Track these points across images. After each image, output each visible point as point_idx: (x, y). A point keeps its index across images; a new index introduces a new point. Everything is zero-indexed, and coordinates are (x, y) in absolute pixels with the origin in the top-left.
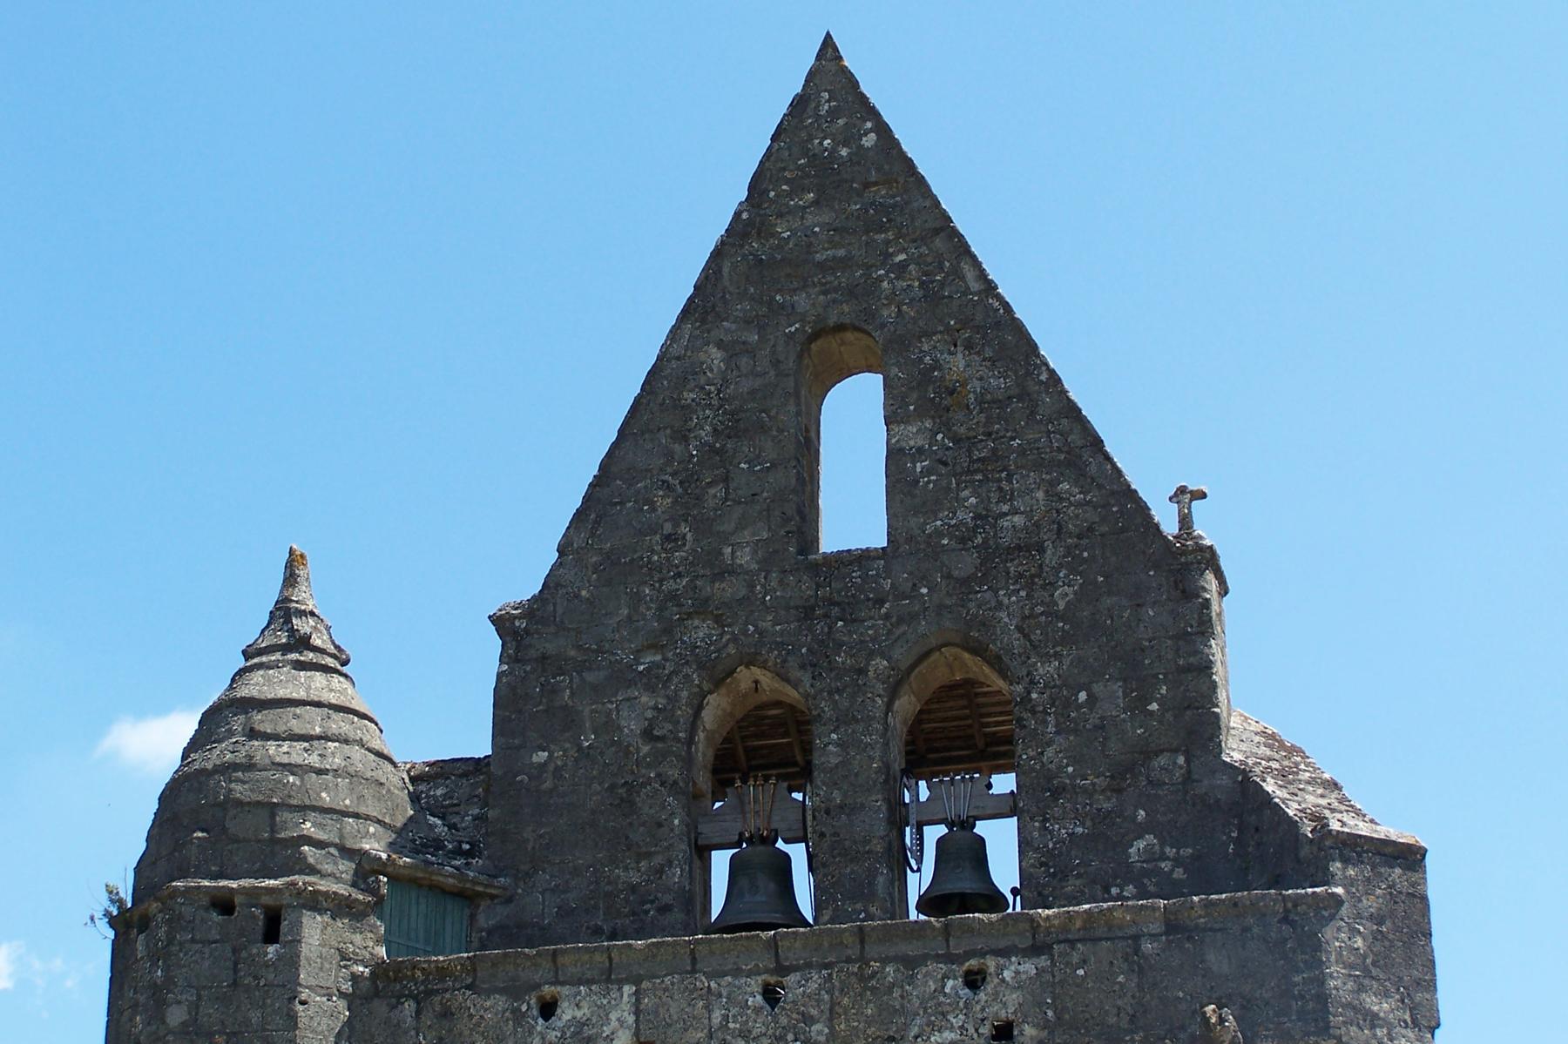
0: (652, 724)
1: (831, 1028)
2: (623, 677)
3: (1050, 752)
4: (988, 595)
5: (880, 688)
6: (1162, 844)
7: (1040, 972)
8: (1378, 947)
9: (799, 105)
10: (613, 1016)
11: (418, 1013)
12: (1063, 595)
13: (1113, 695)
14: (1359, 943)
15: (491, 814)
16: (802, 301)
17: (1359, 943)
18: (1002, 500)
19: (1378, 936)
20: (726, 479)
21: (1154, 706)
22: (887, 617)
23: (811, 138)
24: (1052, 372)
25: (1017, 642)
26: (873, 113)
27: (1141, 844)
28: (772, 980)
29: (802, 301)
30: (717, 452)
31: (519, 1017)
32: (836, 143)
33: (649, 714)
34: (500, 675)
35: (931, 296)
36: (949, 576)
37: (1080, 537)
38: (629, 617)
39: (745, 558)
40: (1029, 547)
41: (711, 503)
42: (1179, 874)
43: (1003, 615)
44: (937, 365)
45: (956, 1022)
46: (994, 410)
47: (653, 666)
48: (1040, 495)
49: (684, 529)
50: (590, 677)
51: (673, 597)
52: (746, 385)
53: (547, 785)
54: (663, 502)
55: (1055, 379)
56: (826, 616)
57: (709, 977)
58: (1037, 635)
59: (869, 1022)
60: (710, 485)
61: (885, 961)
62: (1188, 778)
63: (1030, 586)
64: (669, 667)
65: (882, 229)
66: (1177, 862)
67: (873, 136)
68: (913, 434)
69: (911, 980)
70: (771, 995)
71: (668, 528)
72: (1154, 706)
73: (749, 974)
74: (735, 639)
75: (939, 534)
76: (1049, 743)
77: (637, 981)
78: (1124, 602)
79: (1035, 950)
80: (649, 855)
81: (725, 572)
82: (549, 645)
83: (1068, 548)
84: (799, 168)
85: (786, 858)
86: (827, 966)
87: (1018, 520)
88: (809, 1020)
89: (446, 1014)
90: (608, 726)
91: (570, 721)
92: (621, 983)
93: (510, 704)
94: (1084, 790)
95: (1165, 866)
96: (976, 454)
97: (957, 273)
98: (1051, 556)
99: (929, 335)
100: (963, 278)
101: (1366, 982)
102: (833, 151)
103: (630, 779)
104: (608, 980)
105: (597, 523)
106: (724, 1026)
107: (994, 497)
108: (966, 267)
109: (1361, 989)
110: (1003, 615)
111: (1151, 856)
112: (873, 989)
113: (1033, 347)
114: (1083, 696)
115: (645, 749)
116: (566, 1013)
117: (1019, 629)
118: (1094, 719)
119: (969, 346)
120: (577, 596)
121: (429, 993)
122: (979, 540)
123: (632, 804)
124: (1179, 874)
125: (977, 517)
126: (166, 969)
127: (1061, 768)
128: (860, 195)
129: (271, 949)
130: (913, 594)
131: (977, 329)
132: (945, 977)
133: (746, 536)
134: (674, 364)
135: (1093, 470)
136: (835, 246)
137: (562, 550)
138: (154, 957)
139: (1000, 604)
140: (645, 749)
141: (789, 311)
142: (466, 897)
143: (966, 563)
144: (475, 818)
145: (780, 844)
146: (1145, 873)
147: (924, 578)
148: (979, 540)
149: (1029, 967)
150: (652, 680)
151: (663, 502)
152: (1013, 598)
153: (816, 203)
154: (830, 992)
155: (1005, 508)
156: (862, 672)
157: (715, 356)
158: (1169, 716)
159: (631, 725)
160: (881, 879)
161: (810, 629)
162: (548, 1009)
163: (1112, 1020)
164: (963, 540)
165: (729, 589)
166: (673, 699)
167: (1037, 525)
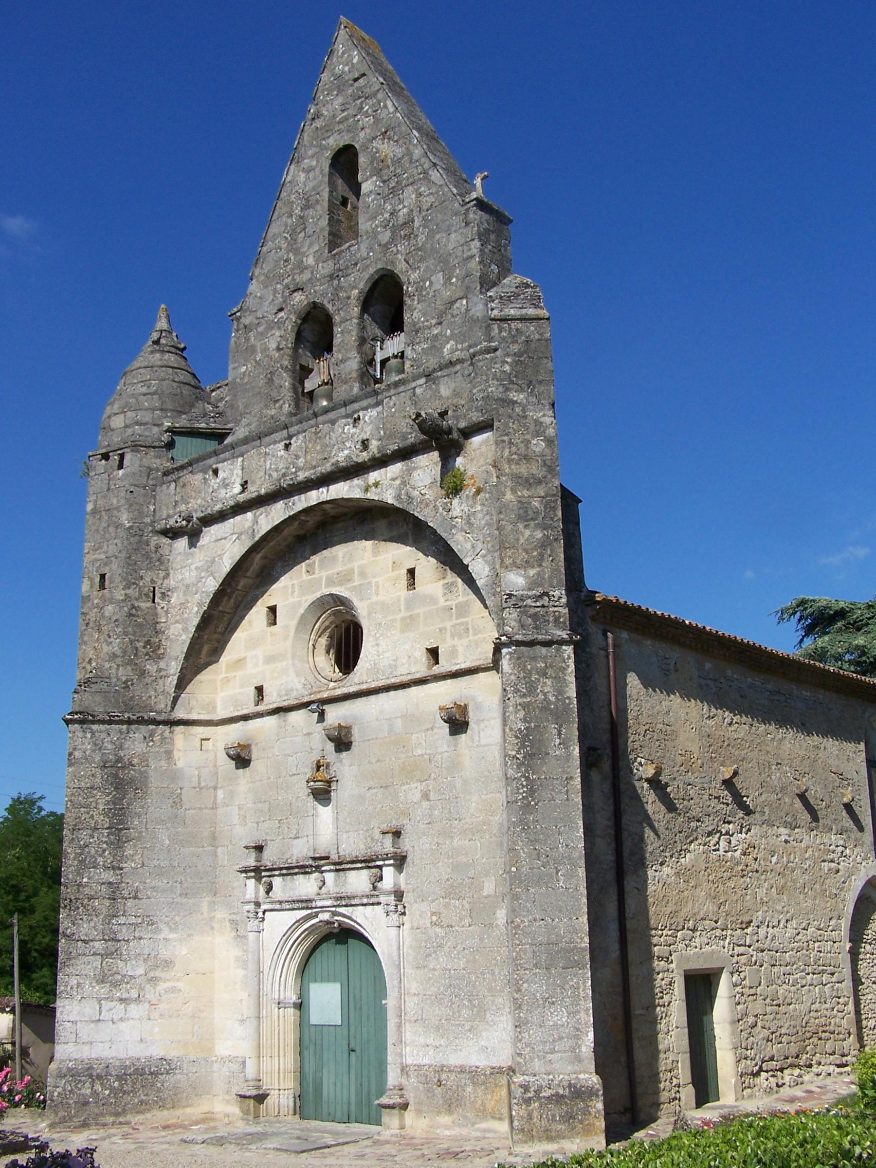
8: (519, 368)
10: (235, 472)
12: (422, 238)
14: (507, 368)
17: (507, 368)
21: (454, 280)
27: (448, 346)
28: (287, 442)
32: (344, 66)
33: (279, 339)
36: (380, 245)
38: (273, 300)
45: (348, 445)
50: (260, 329)
52: (311, 184)
53: (246, 381)
62: (467, 310)
69: (333, 430)
70: (287, 447)
73: (279, 442)
75: (377, 226)
87: (405, 210)
90: (266, 349)
92: (238, 457)
96: (391, 186)
101: (511, 386)
103: (271, 369)
104: (234, 457)
109: (507, 389)
114: (428, 283)
115: (277, 355)
116: (221, 474)
117: (405, 260)
122: (391, 225)
127: (419, 319)
128: (352, 85)
129: (121, 472)
148: (391, 225)
154: (305, 443)
155: (401, 207)
158: (460, 283)
162: (216, 472)
164: (385, 227)
165: (306, 276)
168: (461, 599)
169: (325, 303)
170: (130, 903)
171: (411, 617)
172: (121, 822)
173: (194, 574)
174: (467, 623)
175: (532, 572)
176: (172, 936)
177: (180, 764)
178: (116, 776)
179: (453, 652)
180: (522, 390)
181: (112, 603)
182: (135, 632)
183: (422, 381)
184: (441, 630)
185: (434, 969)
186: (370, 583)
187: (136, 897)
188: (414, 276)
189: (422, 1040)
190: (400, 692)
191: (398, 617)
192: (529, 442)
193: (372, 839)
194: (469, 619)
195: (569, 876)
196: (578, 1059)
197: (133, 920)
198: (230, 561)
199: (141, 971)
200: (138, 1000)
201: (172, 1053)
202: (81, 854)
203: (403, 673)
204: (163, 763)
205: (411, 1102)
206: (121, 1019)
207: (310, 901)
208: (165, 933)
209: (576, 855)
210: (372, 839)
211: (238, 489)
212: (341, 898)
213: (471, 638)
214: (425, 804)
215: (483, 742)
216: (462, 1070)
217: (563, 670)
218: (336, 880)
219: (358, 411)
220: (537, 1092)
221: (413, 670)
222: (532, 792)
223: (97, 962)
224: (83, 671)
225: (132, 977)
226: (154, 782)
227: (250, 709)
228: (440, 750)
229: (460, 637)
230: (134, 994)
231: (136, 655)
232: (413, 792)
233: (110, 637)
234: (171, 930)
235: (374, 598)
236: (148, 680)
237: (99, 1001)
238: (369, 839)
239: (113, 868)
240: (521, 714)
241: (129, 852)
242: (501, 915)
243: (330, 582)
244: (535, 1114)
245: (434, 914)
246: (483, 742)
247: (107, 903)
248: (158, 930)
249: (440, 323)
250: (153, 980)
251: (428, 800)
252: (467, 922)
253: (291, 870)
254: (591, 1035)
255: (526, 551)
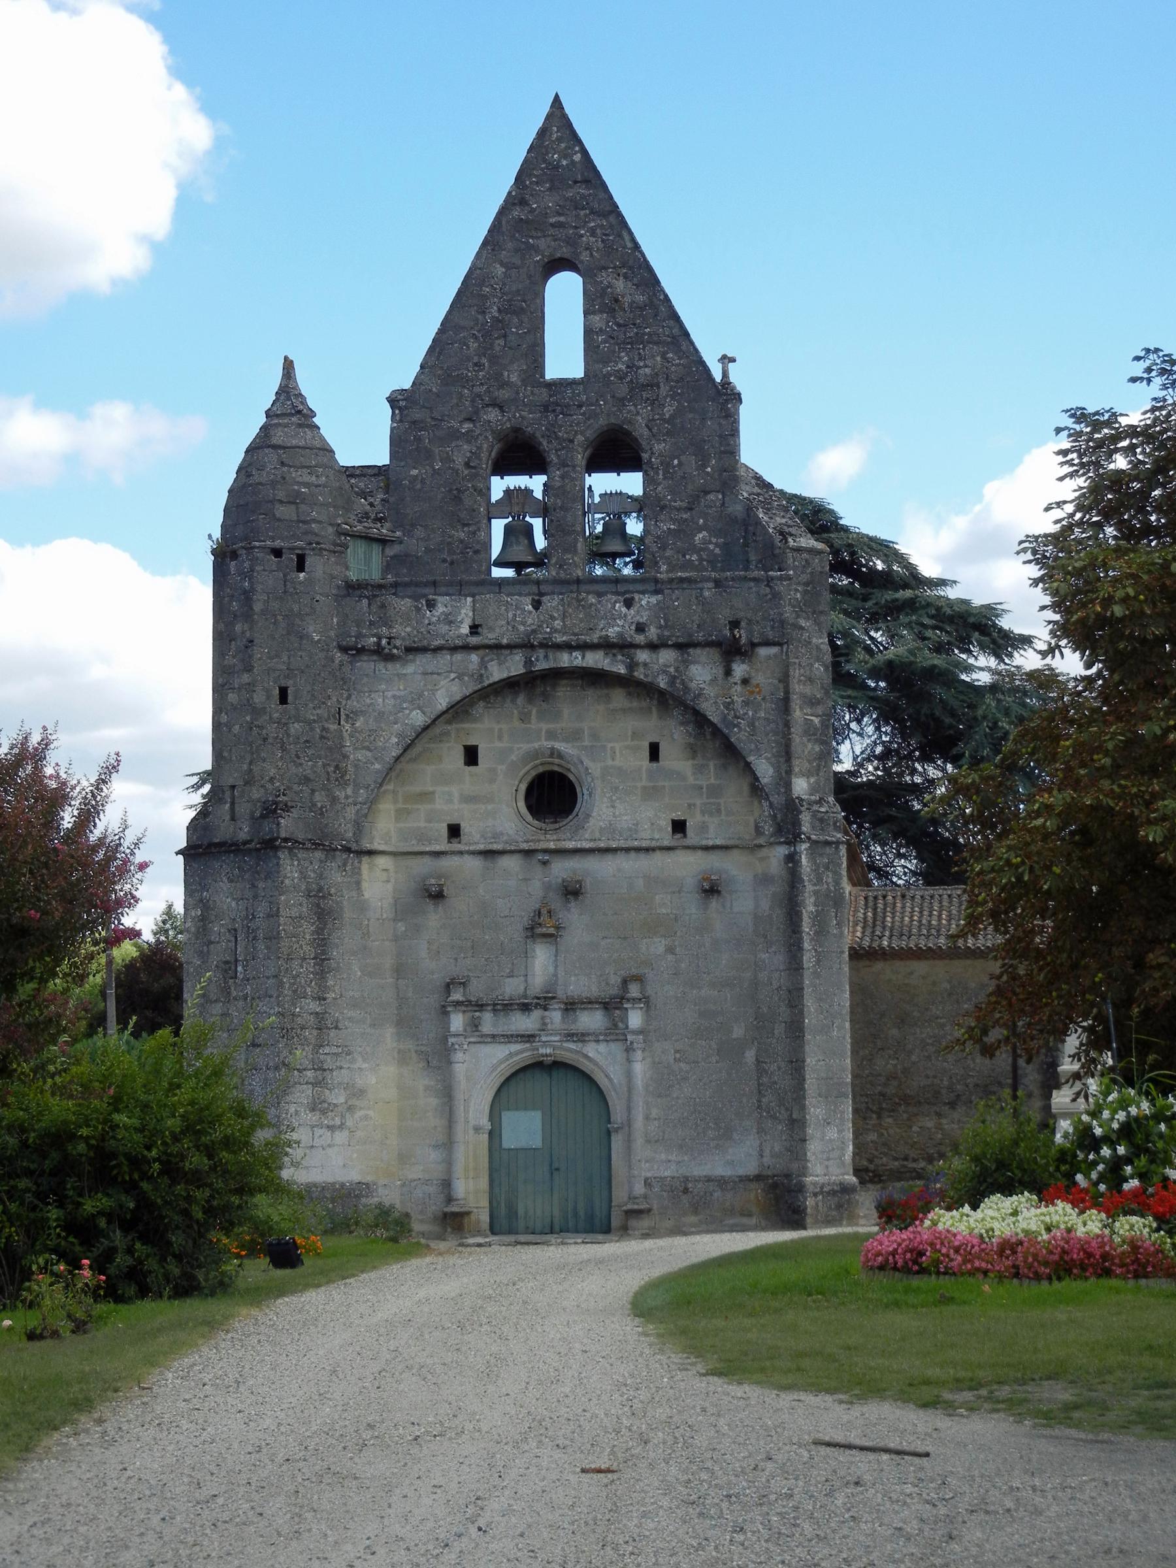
0: (469, 459)
1: (564, 622)
2: (455, 435)
3: (660, 488)
4: (632, 408)
5: (580, 450)
6: (710, 536)
7: (659, 602)
9: (542, 133)
10: (463, 611)
11: (370, 604)
13: (691, 461)
14: (798, 595)
15: (392, 500)
16: (542, 243)
18: (640, 359)
19: (805, 592)
20: (505, 336)
21: (709, 469)
22: (583, 414)
23: (547, 154)
24: (666, 296)
25: (646, 432)
26: (580, 142)
29: (542, 243)
30: (500, 321)
31: (418, 609)
33: (468, 454)
34: (392, 429)
35: (609, 249)
36: (613, 397)
37: (677, 382)
39: (514, 378)
40: (652, 385)
41: (497, 348)
42: (717, 551)
43: (639, 418)
44: (610, 286)
46: (634, 310)
47: (469, 431)
48: (659, 359)
49: (484, 360)
51: (479, 396)
53: (419, 486)
54: (473, 345)
55: (667, 299)
56: (554, 411)
57: (508, 595)
58: (655, 430)
59: (581, 621)
60: (497, 338)
61: (588, 593)
63: (652, 404)
64: (478, 432)
65: (583, 209)
66: (716, 545)
67: (579, 155)
68: (598, 320)
71: (476, 359)
72: (709, 469)
74: (509, 420)
76: (659, 484)
77: (473, 596)
78: (697, 417)
79: (657, 592)
80: (468, 525)
81: (504, 384)
82: (417, 414)
83: (671, 387)
84: (542, 169)
85: (530, 528)
86: (561, 594)
87: (647, 370)
88: (553, 618)
89: (383, 606)
90: (448, 459)
91: (429, 455)
92: (466, 596)
93: (397, 442)
94: (675, 508)
95: (711, 547)
97: (620, 236)
98: (664, 390)
99: (605, 268)
100: (623, 239)
102: (559, 161)
105: (440, 353)
106: (514, 619)
107: (636, 358)
108: (625, 234)
109: (798, 616)
110: (639, 418)
111: (705, 542)
112: (583, 606)
113: (658, 282)
114: (676, 462)
117: (647, 426)
118: (680, 473)
119: (626, 277)
120: (430, 391)
121: (375, 596)
123: (460, 499)
124: (717, 551)
125: (628, 367)
126: (251, 583)
129: (302, 575)
130: (597, 404)
131: (631, 268)
132: (616, 602)
133: (515, 366)
134: (478, 271)
135: (684, 348)
136: (560, 214)
137: (422, 367)
138: (241, 573)
139: (638, 413)
140: (466, 472)
141: (536, 249)
142: (383, 542)
143: (623, 390)
144: (383, 500)
145: (528, 519)
146: (702, 549)
147: (602, 396)
148: (628, 379)
149: (654, 600)
150: (469, 437)
151: (473, 345)
152: (645, 411)
153: (550, 189)
155: (642, 364)
156: (572, 441)
157: (500, 270)
159: (459, 461)
160: (579, 545)
161: (547, 417)
163: (689, 626)
166: (479, 448)
167: (656, 374)
168: (712, 781)
169: (538, 435)
170: (333, 1033)
171: (654, 787)
172: (324, 952)
173: (391, 702)
174: (719, 804)
175: (812, 780)
176: (365, 1066)
177: (367, 895)
178: (318, 905)
179: (704, 828)
180: (808, 619)
181: (299, 722)
182: (326, 756)
183: (711, 585)
184: (689, 805)
185: (678, 1098)
186: (604, 747)
187: (336, 1028)
188: (659, 447)
189: (663, 1156)
190: (642, 855)
191: (639, 785)
192: (812, 665)
193: (607, 984)
194: (722, 801)
195: (840, 1028)
196: (843, 1163)
197: (334, 1050)
198: (447, 700)
199: (342, 1100)
200: (341, 1127)
201: (369, 1179)
202: (294, 984)
203: (645, 837)
204: (354, 894)
205: (655, 1207)
206: (329, 1146)
207: (533, 1036)
208: (360, 1063)
209: (844, 1012)
210: (607, 984)
211: (465, 630)
212: (573, 1035)
213: (723, 817)
214: (670, 957)
215: (736, 910)
216: (709, 1179)
217: (840, 865)
218: (563, 1018)
219: (633, 592)
220: (822, 1188)
221: (657, 837)
222: (818, 961)
223: (309, 1090)
224: (262, 790)
225: (335, 1105)
226: (348, 914)
227: (443, 846)
228: (688, 912)
229: (711, 814)
230: (338, 1121)
231: (328, 780)
232: (658, 946)
233: (298, 758)
234: (364, 1060)
235: (610, 762)
236: (339, 807)
237: (313, 1127)
238: (603, 984)
239: (319, 999)
240: (812, 900)
241: (330, 983)
242: (750, 1055)
243: (551, 735)
244: (820, 1204)
245: (677, 1051)
246: (736, 910)
247: (315, 1032)
248: (353, 1061)
249: (691, 509)
250: (351, 1109)
251: (673, 954)
252: (714, 1059)
253: (504, 1007)
254: (851, 1147)
255: (809, 761)
